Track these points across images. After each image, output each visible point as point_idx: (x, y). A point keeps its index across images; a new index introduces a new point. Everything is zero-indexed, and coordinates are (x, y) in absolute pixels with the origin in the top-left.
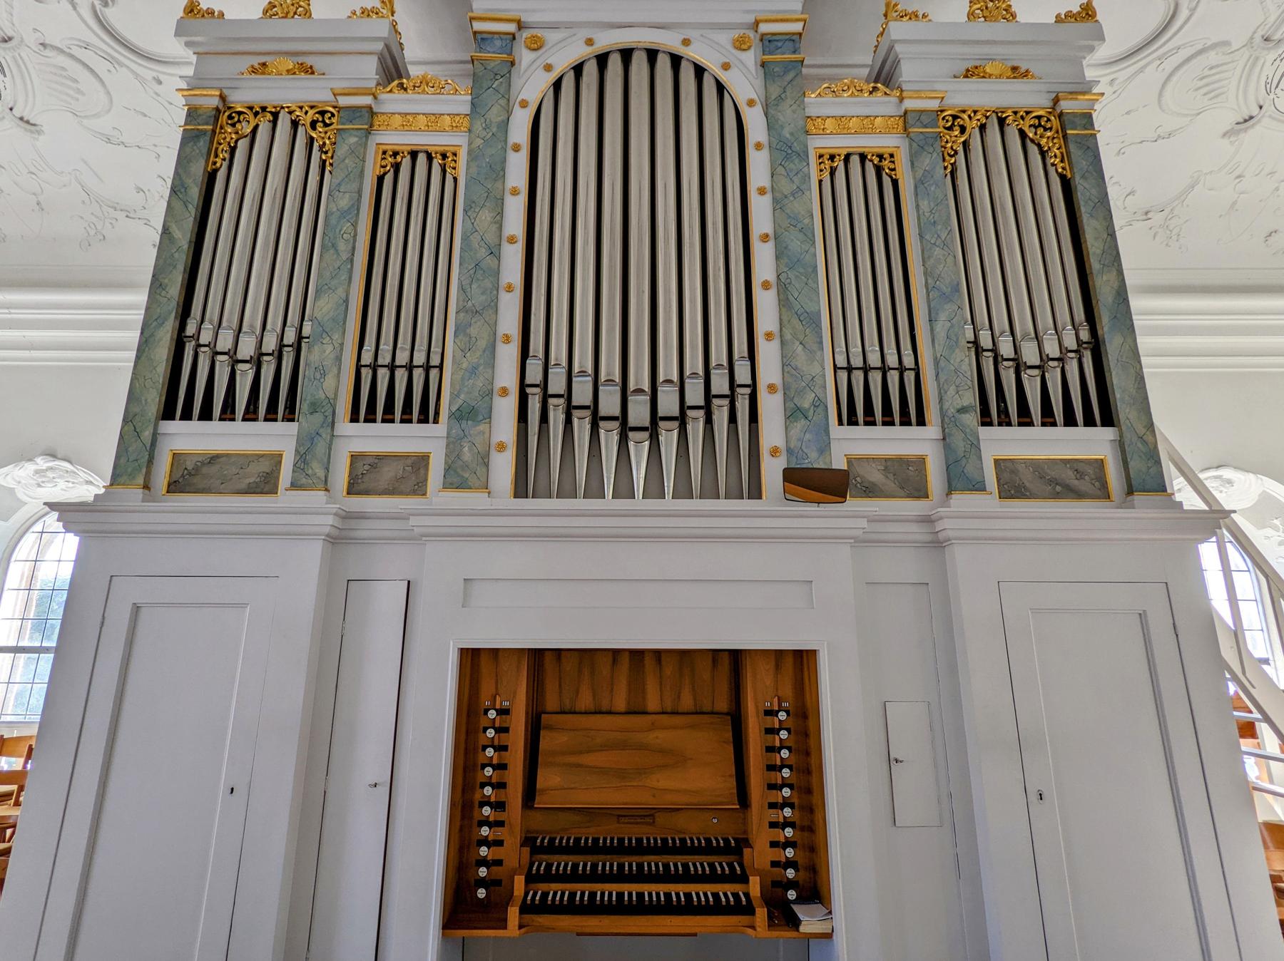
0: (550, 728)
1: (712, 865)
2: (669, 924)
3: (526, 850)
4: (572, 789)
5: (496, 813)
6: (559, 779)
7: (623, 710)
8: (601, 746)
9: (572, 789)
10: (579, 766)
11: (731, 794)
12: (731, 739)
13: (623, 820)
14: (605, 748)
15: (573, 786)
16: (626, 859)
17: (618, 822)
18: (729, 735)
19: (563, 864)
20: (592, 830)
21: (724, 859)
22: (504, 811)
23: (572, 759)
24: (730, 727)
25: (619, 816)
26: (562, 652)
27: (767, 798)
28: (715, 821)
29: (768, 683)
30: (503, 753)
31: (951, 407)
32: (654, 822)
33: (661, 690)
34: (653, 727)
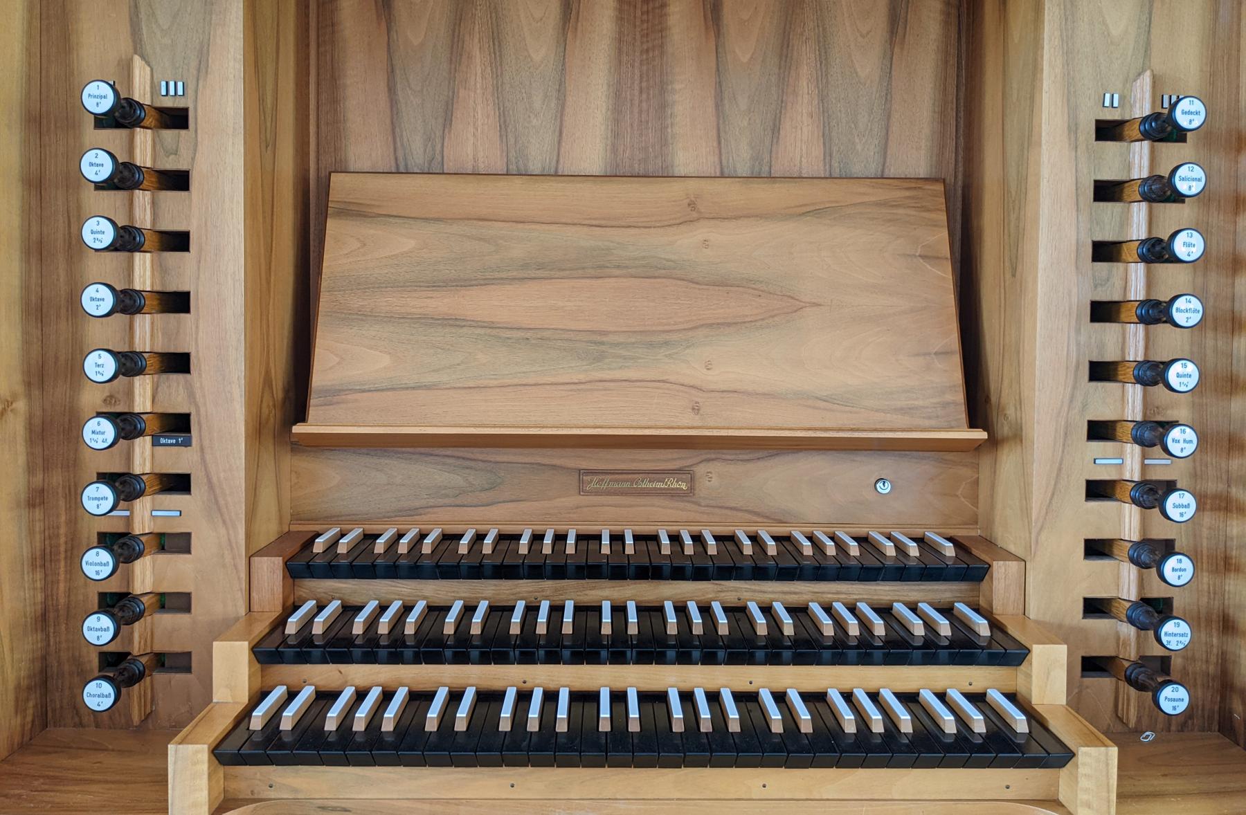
0: (356, 212)
1: (799, 612)
2: (757, 792)
3: (270, 571)
4: (428, 387)
5: (159, 450)
6: (386, 361)
7: (595, 167)
8: (525, 266)
9: (428, 387)
10: (453, 322)
11: (945, 405)
12: (945, 250)
13: (593, 483)
14: (540, 273)
15: (430, 379)
16: (606, 593)
17: (581, 491)
18: (940, 239)
19: (545, 607)
20: (496, 512)
21: (926, 593)
22: (187, 443)
23: (440, 303)
24: (943, 217)
25: (581, 472)
26: (620, 542)
27: (1084, 406)
28: (884, 488)
29: (1116, 32)
30: (173, 257)
31: (917, 254)
32: (692, 489)
33: (719, 106)
34: (693, 213)
